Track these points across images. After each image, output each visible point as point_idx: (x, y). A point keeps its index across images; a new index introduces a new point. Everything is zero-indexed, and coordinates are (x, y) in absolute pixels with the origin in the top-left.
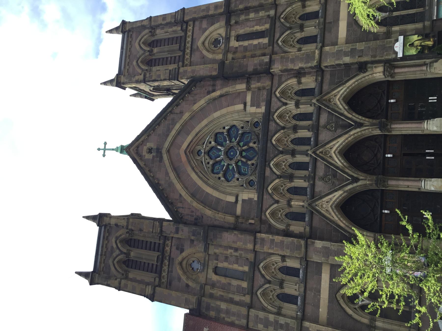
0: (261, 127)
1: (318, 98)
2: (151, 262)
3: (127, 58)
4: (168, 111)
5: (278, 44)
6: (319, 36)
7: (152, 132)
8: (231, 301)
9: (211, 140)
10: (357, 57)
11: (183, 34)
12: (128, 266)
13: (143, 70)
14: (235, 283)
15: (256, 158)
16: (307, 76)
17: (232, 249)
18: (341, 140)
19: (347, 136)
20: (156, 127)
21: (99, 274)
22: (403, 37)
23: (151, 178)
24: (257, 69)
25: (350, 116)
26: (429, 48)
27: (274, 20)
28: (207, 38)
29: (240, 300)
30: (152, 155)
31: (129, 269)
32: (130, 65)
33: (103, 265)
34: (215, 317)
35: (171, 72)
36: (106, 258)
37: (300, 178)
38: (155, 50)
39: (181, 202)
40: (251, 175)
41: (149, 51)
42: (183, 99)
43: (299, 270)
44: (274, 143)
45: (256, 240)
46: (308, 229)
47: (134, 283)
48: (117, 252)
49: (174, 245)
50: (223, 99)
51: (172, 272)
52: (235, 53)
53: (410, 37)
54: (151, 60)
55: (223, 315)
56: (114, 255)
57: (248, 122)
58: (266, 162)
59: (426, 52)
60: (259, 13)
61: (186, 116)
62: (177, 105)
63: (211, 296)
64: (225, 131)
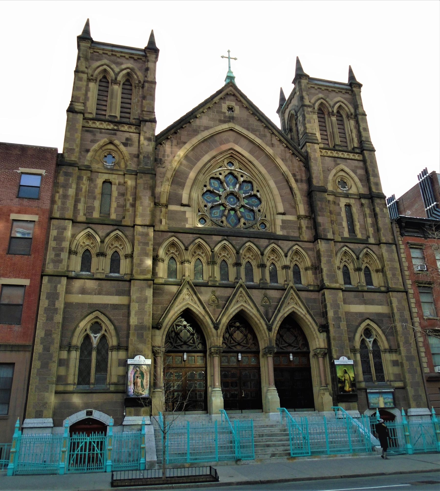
0: (261, 230)
1: (294, 287)
2: (108, 108)
3: (326, 88)
4: (274, 131)
5: (343, 247)
6: (351, 286)
7: (251, 112)
8: (77, 201)
9: (245, 177)
10: (333, 323)
11: (350, 149)
12: (100, 81)
13: (314, 104)
14: (97, 204)
15: (229, 225)
16: (314, 276)
17: (133, 201)
18: (254, 311)
19: (259, 316)
20: (256, 117)
21: (90, 48)
22: (353, 363)
23: (201, 110)
24: (321, 226)
25: (278, 319)
26: (342, 388)
27: (365, 242)
28: (348, 174)
29: (79, 210)
30: (226, 111)
31: (98, 83)
32: (319, 90)
33: (101, 52)
34: (58, 183)
35: (313, 135)
36: (109, 56)
37: (238, 273)
38: (334, 119)
39: (177, 144)
40: (211, 220)
41: (333, 111)
42: (287, 147)
43: (118, 272)
44: (247, 244)
45: (146, 227)
46: (161, 281)
47: (84, 88)
48: (117, 70)
49: (130, 136)
50: (288, 190)
51: (101, 133)
52: (334, 203)
53: (352, 370)
54: (323, 113)
55: (61, 191)
56: (113, 66)
57: (265, 217)
58: (227, 236)
59: (340, 385)
60: (371, 227)
61: (270, 150)
62: (280, 140)
63: (80, 178)
64: (255, 192)
